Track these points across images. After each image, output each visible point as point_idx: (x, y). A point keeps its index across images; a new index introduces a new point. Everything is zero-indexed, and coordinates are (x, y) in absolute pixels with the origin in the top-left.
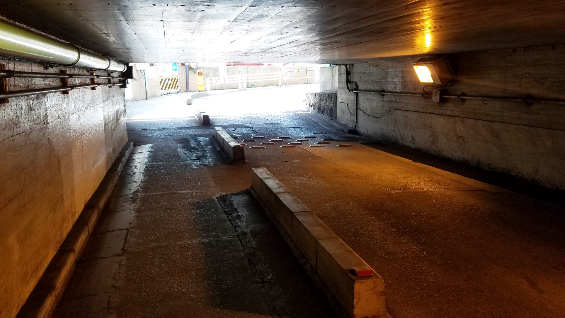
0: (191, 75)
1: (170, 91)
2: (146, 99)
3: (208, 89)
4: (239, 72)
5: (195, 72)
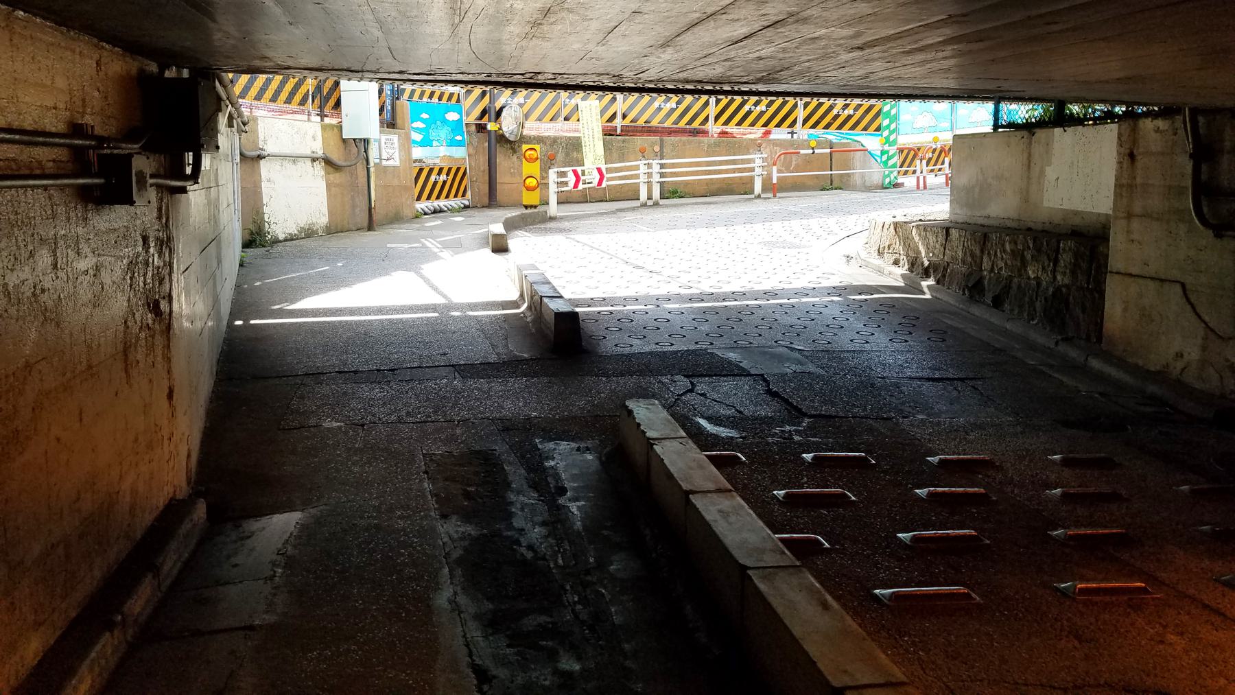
0: (503, 161)
1: (442, 203)
2: (370, 228)
3: (553, 199)
4: (643, 151)
5: (514, 151)
